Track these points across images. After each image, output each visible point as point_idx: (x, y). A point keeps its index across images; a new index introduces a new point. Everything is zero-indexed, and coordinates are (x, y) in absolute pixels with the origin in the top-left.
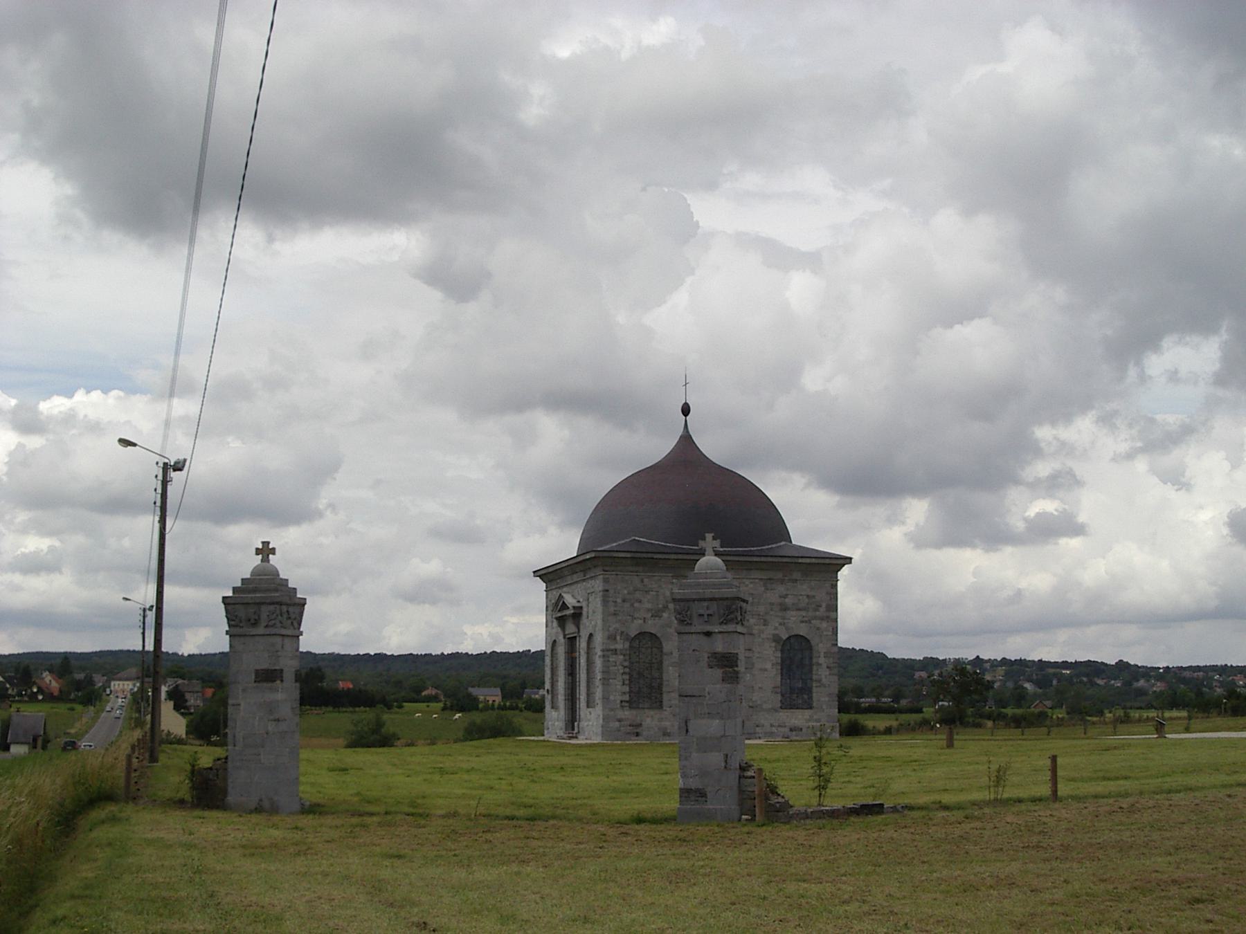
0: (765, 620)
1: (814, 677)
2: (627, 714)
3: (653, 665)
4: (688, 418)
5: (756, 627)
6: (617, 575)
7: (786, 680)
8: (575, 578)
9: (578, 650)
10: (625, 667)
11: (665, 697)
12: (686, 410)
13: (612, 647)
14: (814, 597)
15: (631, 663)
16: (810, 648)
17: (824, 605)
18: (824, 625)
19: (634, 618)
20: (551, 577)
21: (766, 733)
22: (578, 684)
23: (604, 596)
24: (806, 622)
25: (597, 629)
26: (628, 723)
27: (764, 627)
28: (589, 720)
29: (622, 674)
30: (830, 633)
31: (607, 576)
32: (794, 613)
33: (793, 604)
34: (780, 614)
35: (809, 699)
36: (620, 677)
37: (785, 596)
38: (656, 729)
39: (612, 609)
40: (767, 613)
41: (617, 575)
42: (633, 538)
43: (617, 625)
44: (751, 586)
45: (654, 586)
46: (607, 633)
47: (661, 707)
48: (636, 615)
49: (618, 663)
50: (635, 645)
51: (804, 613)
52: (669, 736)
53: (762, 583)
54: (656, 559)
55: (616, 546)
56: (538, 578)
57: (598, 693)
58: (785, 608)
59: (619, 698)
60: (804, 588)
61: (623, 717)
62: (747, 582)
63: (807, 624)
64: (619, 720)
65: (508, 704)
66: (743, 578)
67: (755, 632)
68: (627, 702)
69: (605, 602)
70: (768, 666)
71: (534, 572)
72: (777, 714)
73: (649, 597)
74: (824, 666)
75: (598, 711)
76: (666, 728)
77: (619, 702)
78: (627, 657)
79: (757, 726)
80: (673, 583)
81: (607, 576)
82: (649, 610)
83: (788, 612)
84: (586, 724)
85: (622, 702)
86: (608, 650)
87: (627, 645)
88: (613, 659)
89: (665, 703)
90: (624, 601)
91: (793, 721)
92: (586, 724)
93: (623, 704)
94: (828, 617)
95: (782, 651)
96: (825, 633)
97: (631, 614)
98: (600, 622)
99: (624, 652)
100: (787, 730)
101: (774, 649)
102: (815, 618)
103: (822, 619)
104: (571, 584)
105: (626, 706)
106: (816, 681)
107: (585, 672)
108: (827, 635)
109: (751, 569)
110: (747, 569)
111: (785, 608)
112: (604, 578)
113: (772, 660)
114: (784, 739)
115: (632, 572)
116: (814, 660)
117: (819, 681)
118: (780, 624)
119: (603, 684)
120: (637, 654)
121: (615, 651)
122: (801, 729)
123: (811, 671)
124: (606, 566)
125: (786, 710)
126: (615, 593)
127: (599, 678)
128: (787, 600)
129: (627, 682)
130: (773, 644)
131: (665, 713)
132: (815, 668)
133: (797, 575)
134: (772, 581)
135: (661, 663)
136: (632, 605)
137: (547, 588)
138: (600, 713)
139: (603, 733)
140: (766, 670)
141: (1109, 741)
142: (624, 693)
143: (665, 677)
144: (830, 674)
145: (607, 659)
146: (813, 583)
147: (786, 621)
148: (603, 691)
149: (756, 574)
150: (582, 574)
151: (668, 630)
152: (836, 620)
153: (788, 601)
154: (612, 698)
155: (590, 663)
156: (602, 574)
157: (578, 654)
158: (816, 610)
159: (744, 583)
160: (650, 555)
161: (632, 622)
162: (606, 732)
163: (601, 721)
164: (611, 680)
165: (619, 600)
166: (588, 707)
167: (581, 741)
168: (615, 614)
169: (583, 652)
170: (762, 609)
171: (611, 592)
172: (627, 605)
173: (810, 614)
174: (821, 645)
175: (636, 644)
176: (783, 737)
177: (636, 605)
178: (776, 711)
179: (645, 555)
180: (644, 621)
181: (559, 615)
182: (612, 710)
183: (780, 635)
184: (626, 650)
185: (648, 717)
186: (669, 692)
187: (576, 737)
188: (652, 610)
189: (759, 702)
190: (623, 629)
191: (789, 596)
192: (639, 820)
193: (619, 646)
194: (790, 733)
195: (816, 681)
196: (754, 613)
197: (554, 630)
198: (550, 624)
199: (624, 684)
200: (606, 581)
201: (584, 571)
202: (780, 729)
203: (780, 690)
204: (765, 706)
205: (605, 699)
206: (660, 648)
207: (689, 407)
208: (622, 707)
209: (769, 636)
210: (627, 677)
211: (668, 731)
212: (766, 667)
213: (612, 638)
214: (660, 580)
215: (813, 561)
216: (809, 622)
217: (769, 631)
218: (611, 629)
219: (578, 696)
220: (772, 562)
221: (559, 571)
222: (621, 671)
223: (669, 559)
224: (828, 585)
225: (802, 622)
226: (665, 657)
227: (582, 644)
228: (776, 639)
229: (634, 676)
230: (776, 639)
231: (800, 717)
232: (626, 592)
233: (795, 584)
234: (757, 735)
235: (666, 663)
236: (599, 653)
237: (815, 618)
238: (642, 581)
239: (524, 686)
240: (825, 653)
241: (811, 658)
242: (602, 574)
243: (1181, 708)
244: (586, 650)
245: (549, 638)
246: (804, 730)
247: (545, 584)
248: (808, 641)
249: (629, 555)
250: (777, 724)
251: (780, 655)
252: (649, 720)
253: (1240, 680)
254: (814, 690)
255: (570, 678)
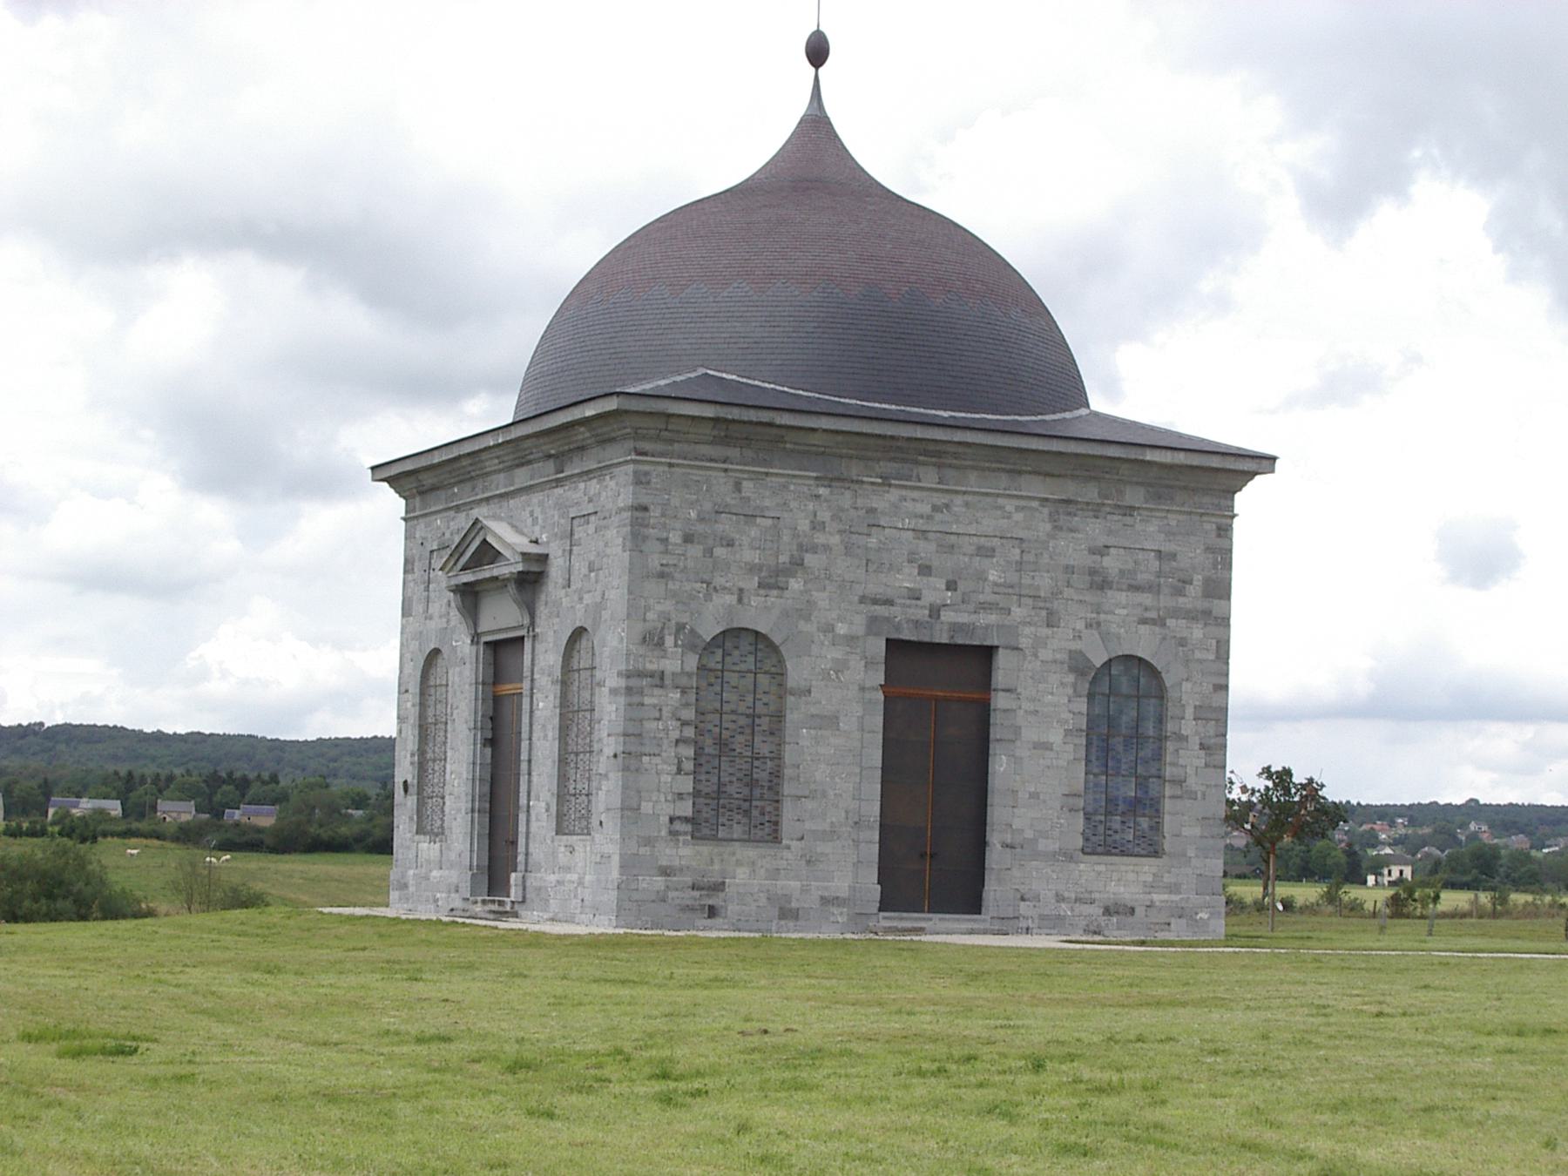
0: (1050, 613)
1: (1169, 772)
2: (685, 854)
3: (757, 721)
4: (821, 70)
5: (1027, 630)
6: (671, 465)
7: (1095, 775)
8: (522, 477)
9: (527, 673)
10: (685, 723)
11: (788, 812)
12: (817, 52)
13: (650, 667)
14: (1173, 556)
15: (700, 713)
16: (1161, 693)
17: (1198, 579)
18: (1197, 632)
19: (712, 589)
20: (428, 480)
21: (1042, 917)
22: (524, 766)
23: (635, 523)
24: (1153, 622)
25: (606, 615)
26: (689, 880)
27: (1049, 631)
28: (568, 869)
29: (677, 741)
30: (1212, 657)
31: (646, 468)
32: (1122, 597)
33: (1122, 572)
34: (1088, 597)
35: (1151, 828)
36: (670, 752)
37: (1103, 550)
38: (763, 902)
39: (655, 562)
40: (1056, 594)
41: (671, 465)
42: (704, 371)
43: (668, 606)
44: (1019, 517)
45: (767, 503)
46: (639, 627)
47: (775, 838)
48: (719, 581)
49: (665, 714)
50: (712, 665)
51: (1146, 599)
52: (797, 918)
53: (1046, 511)
54: (780, 426)
55: (666, 385)
56: (385, 485)
57: (607, 793)
58: (1100, 582)
59: (666, 810)
60: (1150, 532)
61: (676, 863)
62: (1010, 505)
63: (1157, 629)
64: (665, 872)
65: (25, 825)
66: (998, 495)
67: (1024, 642)
68: (686, 820)
69: (637, 538)
70: (1056, 737)
71: (373, 468)
72: (1072, 866)
73: (754, 532)
74: (1194, 742)
75: (606, 841)
76: (788, 898)
77: (665, 820)
78: (692, 698)
79: (1023, 899)
80: (818, 497)
81: (646, 468)
82: (752, 569)
83: (1110, 593)
84: (553, 878)
85: (672, 820)
86: (641, 674)
87: (692, 662)
88: (654, 701)
89: (788, 825)
90: (688, 539)
91: (1112, 887)
92: (553, 878)
93: (678, 826)
94: (1207, 613)
95: (1091, 696)
96: (1198, 655)
97: (706, 577)
98: (617, 596)
99: (684, 681)
100: (1096, 910)
101: (1070, 691)
102: (1176, 613)
103: (1191, 616)
104: (501, 496)
105: (686, 833)
106: (1172, 782)
107: (553, 733)
108: (1201, 661)
109: (1020, 473)
110: (1009, 471)
111: (1100, 582)
112: (635, 472)
113: (1067, 722)
114: (1090, 938)
115: (711, 460)
116: (1170, 727)
117: (1180, 782)
118: (1089, 626)
119: (626, 769)
120: (718, 689)
121: (659, 679)
122: (1132, 911)
123: (1159, 756)
124: (644, 438)
125: (1095, 858)
126: (663, 515)
127: (609, 751)
128: (1107, 562)
129: (689, 766)
130: (1071, 678)
131: (786, 853)
132: (1170, 746)
133: (1135, 496)
134: (1071, 508)
135: (779, 717)
136: (709, 552)
137: (407, 512)
138: (613, 850)
139: (619, 908)
140: (1047, 746)
141: (1442, 946)
142: (680, 796)
143: (789, 755)
144: (1207, 765)
145: (636, 699)
146: (1173, 520)
147: (1102, 616)
148: (625, 788)
149: (1036, 487)
150: (550, 466)
151: (802, 626)
152: (1225, 622)
153: (1112, 563)
154: (646, 807)
155: (571, 716)
156: (634, 461)
157: (526, 685)
158: (1179, 592)
159: (1001, 508)
160: (765, 416)
161: (708, 597)
162: (629, 903)
163: (615, 874)
164: (645, 759)
165: (675, 538)
166: (559, 831)
167: (532, 921)
168: (662, 575)
169: (543, 681)
170: (1044, 582)
171: (655, 512)
172: (695, 550)
173: (1166, 601)
174: (1186, 686)
175: (714, 661)
176: (1086, 931)
177: (720, 552)
178: (1070, 858)
179: (753, 415)
180: (740, 600)
181: (468, 577)
182: (648, 841)
183: (1089, 656)
184: (689, 675)
185: (739, 863)
186: (799, 798)
187: (516, 915)
188: (760, 568)
189: (1029, 834)
190: (685, 619)
191: (1112, 550)
192: (332, 1098)
193: (671, 665)
194: (1103, 920)
195: (1172, 782)
196: (1024, 592)
197: (435, 624)
198: (418, 608)
199: (679, 771)
200: (640, 480)
201: (560, 459)
202: (1080, 908)
203: (1082, 804)
204: (1043, 845)
205: (629, 811)
206: (779, 675)
207: (826, 42)
208: (673, 833)
209: (1058, 656)
210: (689, 752)
211: (794, 905)
212: (1052, 739)
213: (653, 640)
214: (785, 487)
215: (1181, 458)
216: (1160, 622)
217: (1059, 643)
218: (650, 616)
219: (523, 801)
220: (1077, 455)
221: (465, 462)
222: (675, 735)
223: (813, 430)
224: (1210, 527)
225: (1144, 621)
226: (791, 699)
227: (544, 659)
228: (1078, 665)
229: (707, 750)
230: (1078, 665)
231: (1131, 876)
232: (693, 514)
233: (1128, 520)
234: (1023, 924)
235: (792, 717)
236: (613, 681)
237: (1176, 613)
238: (738, 486)
239: (47, 789)
240: (1195, 707)
241: (1160, 721)
242: (634, 461)
243: (1317, 878)
244: (558, 673)
245: (414, 645)
246: (1140, 911)
247: (403, 502)
248: (1154, 673)
249: (709, 411)
250: (1073, 896)
251: (1084, 708)
252: (742, 874)
253: (1383, 831)
254: (1168, 805)
255: (488, 751)
